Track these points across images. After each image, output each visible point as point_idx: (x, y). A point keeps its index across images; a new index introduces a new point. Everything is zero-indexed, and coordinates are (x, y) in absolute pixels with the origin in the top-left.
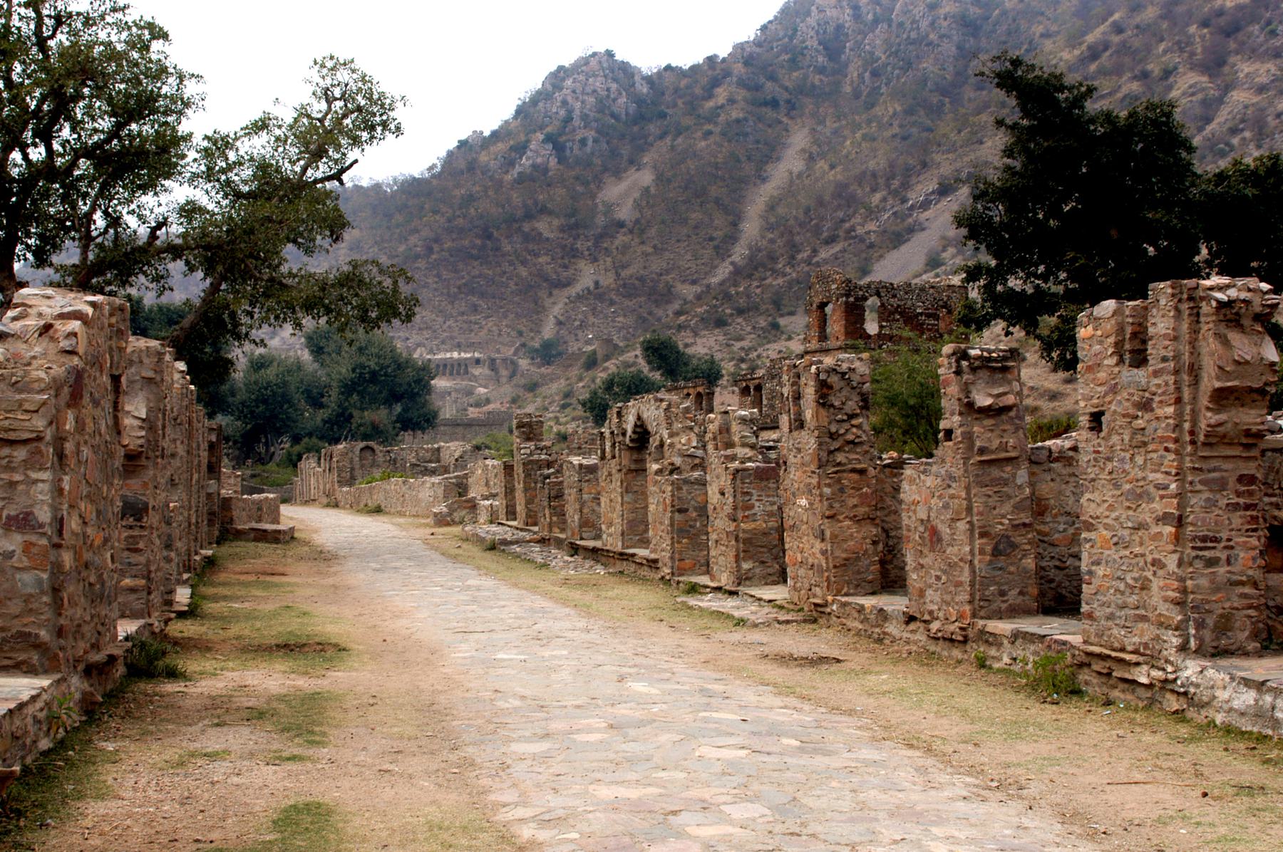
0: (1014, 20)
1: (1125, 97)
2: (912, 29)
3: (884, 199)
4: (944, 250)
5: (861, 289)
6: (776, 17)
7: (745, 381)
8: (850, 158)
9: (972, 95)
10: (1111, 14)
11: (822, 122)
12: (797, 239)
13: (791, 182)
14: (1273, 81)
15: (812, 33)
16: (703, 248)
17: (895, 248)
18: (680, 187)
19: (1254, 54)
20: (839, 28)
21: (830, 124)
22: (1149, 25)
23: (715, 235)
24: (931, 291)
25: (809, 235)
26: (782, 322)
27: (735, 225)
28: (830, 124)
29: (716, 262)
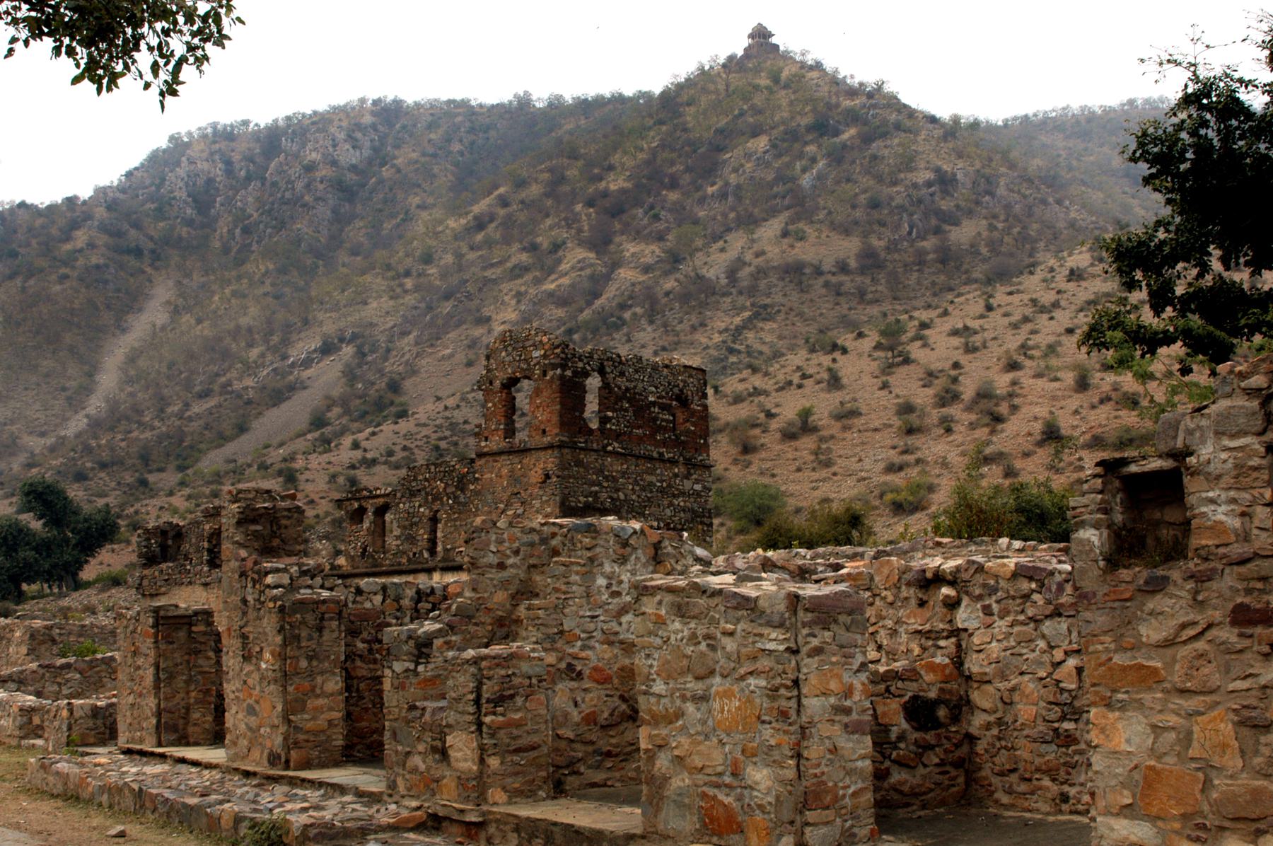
0: (391, 190)
1: (515, 267)
2: (287, 189)
3: (263, 355)
4: (329, 408)
5: (581, 360)
6: (142, 165)
7: (357, 499)
8: (220, 313)
9: (346, 260)
10: (497, 188)
11: (188, 275)
12: (165, 391)
13: (154, 334)
14: (657, 262)
15: (181, 184)
16: (54, 398)
17: (274, 405)
18: (30, 331)
19: (638, 235)
20: (210, 181)
21: (197, 278)
22: (533, 201)
23: (67, 385)
24: (666, 371)
25: (178, 388)
26: (152, 478)
27: (90, 375)
28: (197, 278)
29: (68, 414)
